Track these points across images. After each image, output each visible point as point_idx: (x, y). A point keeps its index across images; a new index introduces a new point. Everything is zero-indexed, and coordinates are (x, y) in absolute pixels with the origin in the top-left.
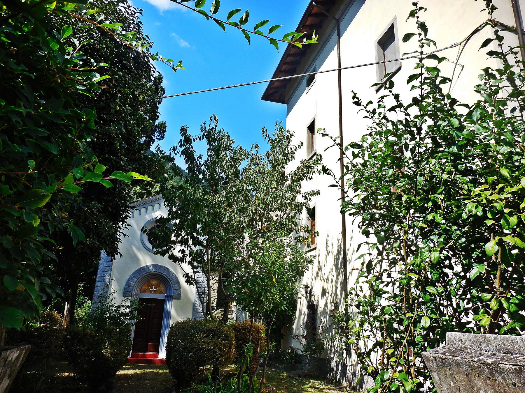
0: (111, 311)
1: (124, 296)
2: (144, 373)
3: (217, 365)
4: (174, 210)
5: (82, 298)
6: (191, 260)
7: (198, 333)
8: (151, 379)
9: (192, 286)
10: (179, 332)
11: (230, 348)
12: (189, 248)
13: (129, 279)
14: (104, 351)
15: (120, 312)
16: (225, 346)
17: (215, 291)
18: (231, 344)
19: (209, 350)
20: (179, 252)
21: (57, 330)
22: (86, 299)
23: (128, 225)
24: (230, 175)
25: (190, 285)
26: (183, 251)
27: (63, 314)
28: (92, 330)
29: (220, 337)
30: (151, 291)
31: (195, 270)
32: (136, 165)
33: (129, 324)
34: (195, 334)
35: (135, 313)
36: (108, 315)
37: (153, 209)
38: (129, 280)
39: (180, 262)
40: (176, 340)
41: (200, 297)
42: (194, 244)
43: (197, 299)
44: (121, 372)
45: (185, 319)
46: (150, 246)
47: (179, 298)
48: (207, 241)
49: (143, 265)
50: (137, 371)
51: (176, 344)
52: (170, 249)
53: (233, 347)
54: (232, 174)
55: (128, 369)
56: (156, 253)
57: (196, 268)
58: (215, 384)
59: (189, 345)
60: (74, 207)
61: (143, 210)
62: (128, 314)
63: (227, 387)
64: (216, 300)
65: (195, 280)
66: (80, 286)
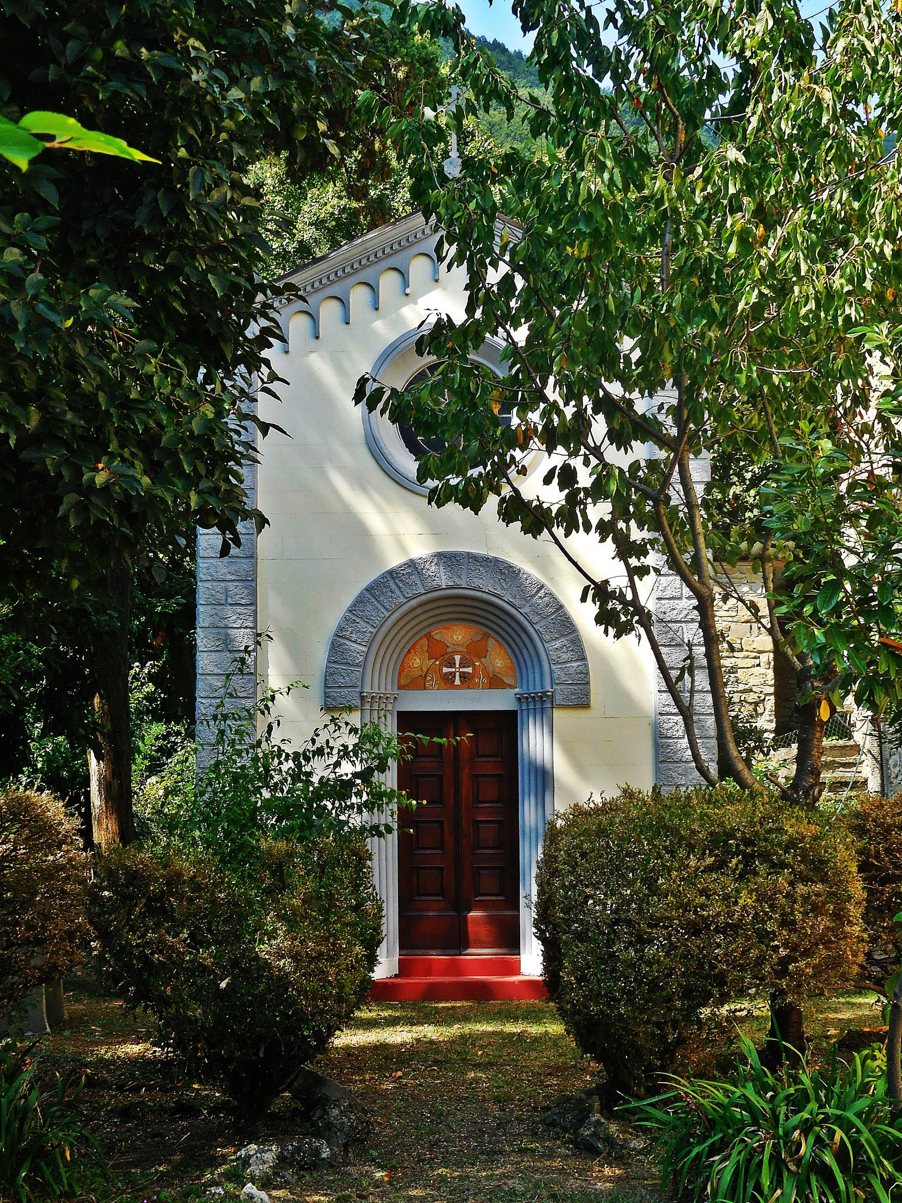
0: (277, 778)
1: (327, 708)
2: (463, 1039)
3: (783, 992)
4: (493, 277)
5: (159, 728)
6: (607, 518)
7: (672, 853)
8: (491, 1064)
9: (629, 639)
10: (583, 855)
11: (840, 916)
12: (594, 461)
13: (341, 629)
14: (263, 950)
15: (315, 779)
16: (817, 909)
17: (764, 658)
18: (840, 898)
19: (732, 929)
20: (547, 480)
21: (63, 868)
22: (178, 733)
23: (273, 377)
24: (754, 54)
25: (618, 636)
26: (567, 476)
27: (88, 803)
28: (201, 861)
29: (783, 865)
30: (447, 681)
31: (634, 562)
32: (265, 81)
33: (363, 828)
34: (660, 856)
35: (389, 780)
36: (266, 794)
37: (406, 284)
38: (339, 634)
39: (559, 532)
40: (573, 887)
41: (671, 688)
42: (618, 438)
43: (667, 698)
44: (346, 1038)
45: (613, 794)
46: (409, 465)
47: (583, 703)
48: (675, 412)
49: (395, 560)
50: (430, 1032)
51: (575, 907)
52: (501, 470)
53: (855, 912)
54: (763, 45)
55: (392, 1022)
56: (438, 498)
57: (641, 550)
58: (779, 1079)
59: (640, 910)
60: (15, 322)
61: (359, 296)
62: (349, 784)
63: (836, 1089)
64: (770, 703)
65: (639, 610)
66: (136, 677)
